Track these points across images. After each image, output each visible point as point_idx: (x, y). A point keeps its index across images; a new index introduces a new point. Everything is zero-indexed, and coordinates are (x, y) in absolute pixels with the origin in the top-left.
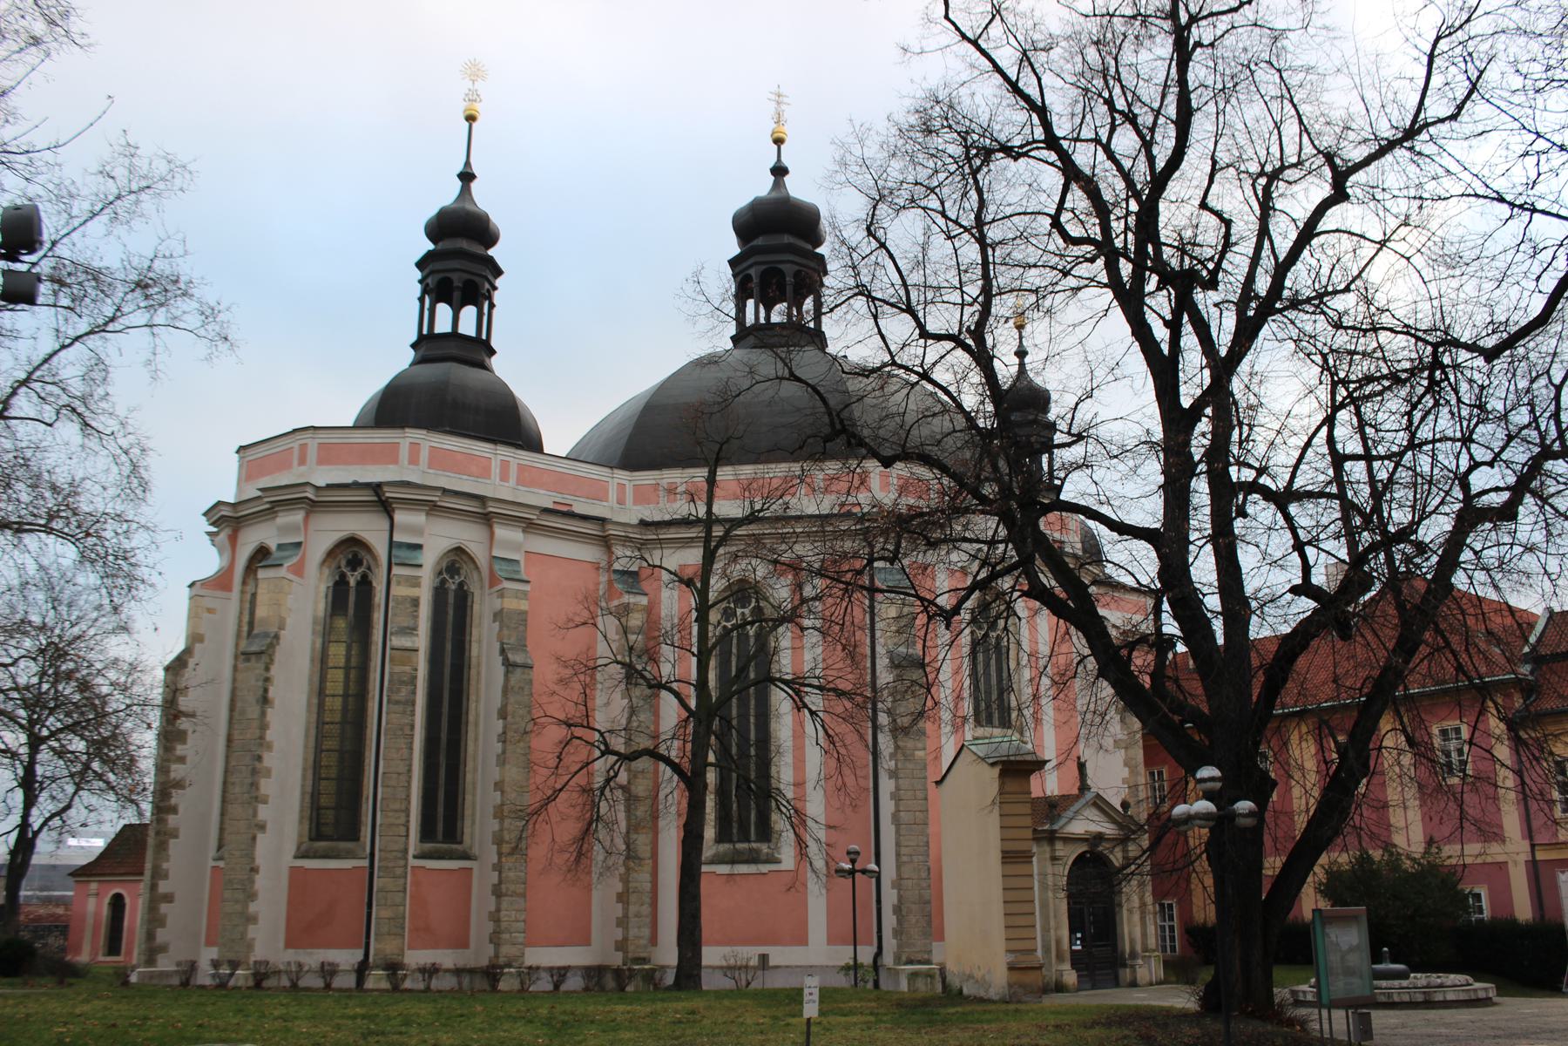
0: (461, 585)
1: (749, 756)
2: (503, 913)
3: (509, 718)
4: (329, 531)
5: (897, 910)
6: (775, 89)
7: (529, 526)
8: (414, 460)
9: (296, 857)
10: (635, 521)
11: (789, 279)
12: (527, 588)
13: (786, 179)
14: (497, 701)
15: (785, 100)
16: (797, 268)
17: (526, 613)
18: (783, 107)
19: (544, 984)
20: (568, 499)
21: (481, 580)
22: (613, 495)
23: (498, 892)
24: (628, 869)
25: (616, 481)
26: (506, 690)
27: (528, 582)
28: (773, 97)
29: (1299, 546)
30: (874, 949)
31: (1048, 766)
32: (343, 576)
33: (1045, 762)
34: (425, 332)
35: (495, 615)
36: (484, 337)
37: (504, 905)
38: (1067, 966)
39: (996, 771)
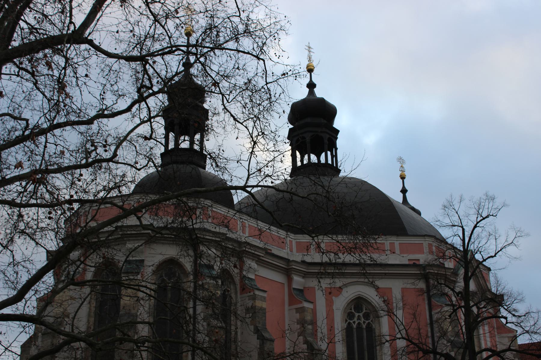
1: (21, 7)
6: (307, 44)
7: (260, 262)
11: (326, 141)
12: (265, 295)
13: (315, 90)
15: (312, 50)
16: (328, 136)
17: (265, 309)
18: (312, 54)
21: (236, 289)
28: (307, 48)
29: (130, 142)
32: (349, 323)
34: (299, 164)
35: (248, 310)
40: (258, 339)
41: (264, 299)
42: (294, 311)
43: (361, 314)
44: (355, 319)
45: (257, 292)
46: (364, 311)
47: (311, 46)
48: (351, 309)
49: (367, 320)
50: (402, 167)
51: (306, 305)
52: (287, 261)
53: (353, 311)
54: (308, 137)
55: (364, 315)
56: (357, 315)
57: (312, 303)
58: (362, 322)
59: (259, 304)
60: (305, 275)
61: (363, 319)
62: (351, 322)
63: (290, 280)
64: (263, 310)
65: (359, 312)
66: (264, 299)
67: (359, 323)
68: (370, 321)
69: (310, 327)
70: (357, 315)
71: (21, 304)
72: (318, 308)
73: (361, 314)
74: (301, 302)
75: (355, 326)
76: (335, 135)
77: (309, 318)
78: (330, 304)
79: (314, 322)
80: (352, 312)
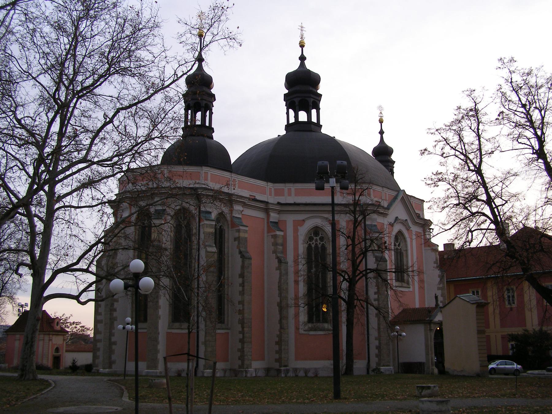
0: (220, 227)
2: (245, 349)
3: (245, 278)
4: (174, 206)
5: (378, 348)
6: (300, 25)
7: (244, 205)
8: (290, 194)
9: (168, 329)
10: (276, 203)
12: (247, 229)
14: (238, 270)
15: (304, 29)
16: (312, 100)
17: (246, 238)
19: (302, 374)
20: (254, 194)
22: (268, 192)
23: (242, 341)
24: (281, 333)
25: (269, 187)
26: (243, 267)
27: (247, 226)
28: (300, 28)
30: (366, 361)
31: (490, 304)
32: (310, 244)
33: (489, 303)
35: (235, 239)
36: (207, 124)
37: (245, 346)
38: (434, 367)
39: (475, 306)
40: (241, 257)
41: (246, 231)
42: (271, 236)
43: (318, 238)
44: (314, 241)
45: (241, 228)
46: (320, 236)
47: (303, 25)
48: (311, 235)
49: (322, 241)
50: (381, 113)
51: (278, 233)
52: (267, 203)
53: (312, 235)
54: (297, 100)
55: (320, 239)
56: (315, 238)
57: (283, 231)
58: (318, 243)
59: (242, 235)
60: (280, 212)
61: (319, 241)
62: (311, 243)
63: (268, 216)
64: (246, 239)
65: (316, 236)
66: (246, 231)
67: (316, 244)
68: (324, 242)
69: (281, 247)
70: (315, 238)
71: (78, 265)
72: (288, 234)
73: (318, 238)
74: (275, 231)
75: (313, 246)
76: (318, 98)
77: (280, 241)
78: (296, 231)
79: (284, 245)
80: (312, 237)
